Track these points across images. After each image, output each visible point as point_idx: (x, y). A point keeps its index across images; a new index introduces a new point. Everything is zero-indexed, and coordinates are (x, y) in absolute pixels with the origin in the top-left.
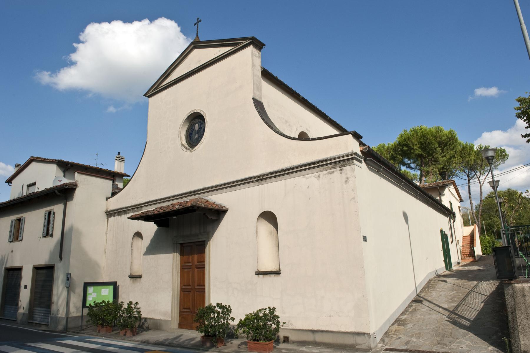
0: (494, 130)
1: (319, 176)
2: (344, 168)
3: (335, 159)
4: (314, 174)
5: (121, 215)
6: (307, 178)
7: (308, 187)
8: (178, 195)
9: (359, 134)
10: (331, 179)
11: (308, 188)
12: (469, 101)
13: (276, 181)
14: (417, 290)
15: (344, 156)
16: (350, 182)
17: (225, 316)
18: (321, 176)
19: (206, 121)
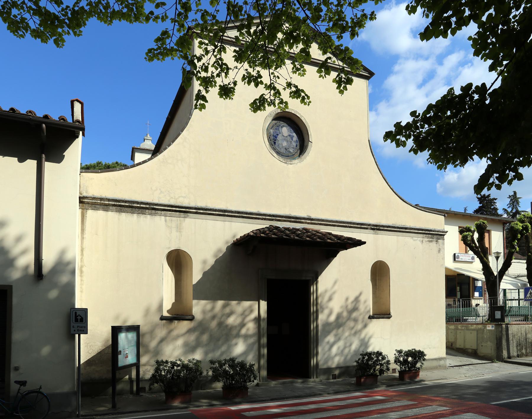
0: (202, 278)
1: (422, 241)
2: (439, 240)
3: (433, 231)
4: (419, 239)
5: (98, 209)
6: (414, 240)
7: (414, 248)
8: (270, 215)
9: (176, 98)
10: (430, 246)
11: (415, 249)
12: (494, 6)
13: (369, 233)
14: (498, 268)
15: (433, 231)
16: (441, 252)
17: (232, 382)
18: (424, 241)
19: (309, 134)
